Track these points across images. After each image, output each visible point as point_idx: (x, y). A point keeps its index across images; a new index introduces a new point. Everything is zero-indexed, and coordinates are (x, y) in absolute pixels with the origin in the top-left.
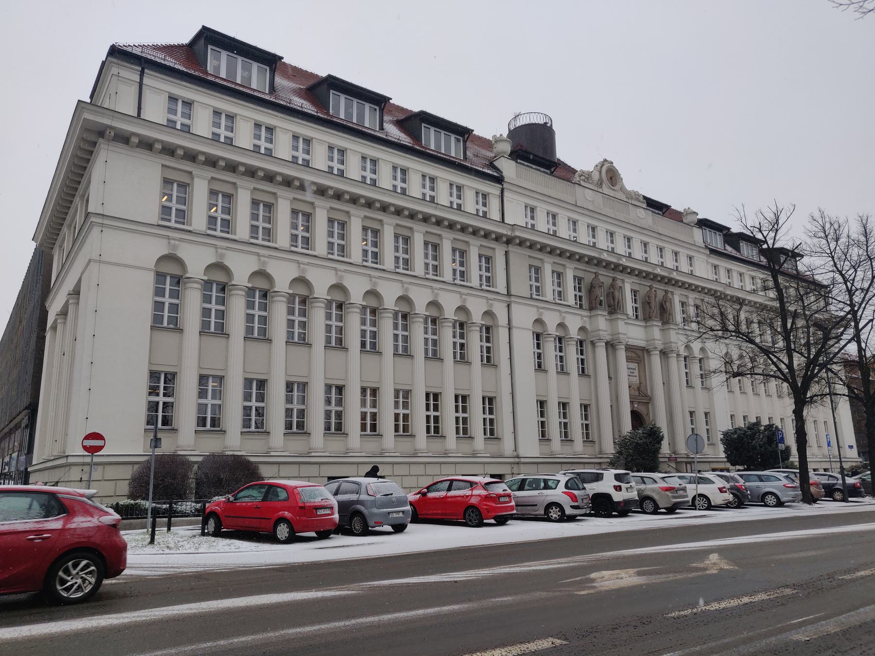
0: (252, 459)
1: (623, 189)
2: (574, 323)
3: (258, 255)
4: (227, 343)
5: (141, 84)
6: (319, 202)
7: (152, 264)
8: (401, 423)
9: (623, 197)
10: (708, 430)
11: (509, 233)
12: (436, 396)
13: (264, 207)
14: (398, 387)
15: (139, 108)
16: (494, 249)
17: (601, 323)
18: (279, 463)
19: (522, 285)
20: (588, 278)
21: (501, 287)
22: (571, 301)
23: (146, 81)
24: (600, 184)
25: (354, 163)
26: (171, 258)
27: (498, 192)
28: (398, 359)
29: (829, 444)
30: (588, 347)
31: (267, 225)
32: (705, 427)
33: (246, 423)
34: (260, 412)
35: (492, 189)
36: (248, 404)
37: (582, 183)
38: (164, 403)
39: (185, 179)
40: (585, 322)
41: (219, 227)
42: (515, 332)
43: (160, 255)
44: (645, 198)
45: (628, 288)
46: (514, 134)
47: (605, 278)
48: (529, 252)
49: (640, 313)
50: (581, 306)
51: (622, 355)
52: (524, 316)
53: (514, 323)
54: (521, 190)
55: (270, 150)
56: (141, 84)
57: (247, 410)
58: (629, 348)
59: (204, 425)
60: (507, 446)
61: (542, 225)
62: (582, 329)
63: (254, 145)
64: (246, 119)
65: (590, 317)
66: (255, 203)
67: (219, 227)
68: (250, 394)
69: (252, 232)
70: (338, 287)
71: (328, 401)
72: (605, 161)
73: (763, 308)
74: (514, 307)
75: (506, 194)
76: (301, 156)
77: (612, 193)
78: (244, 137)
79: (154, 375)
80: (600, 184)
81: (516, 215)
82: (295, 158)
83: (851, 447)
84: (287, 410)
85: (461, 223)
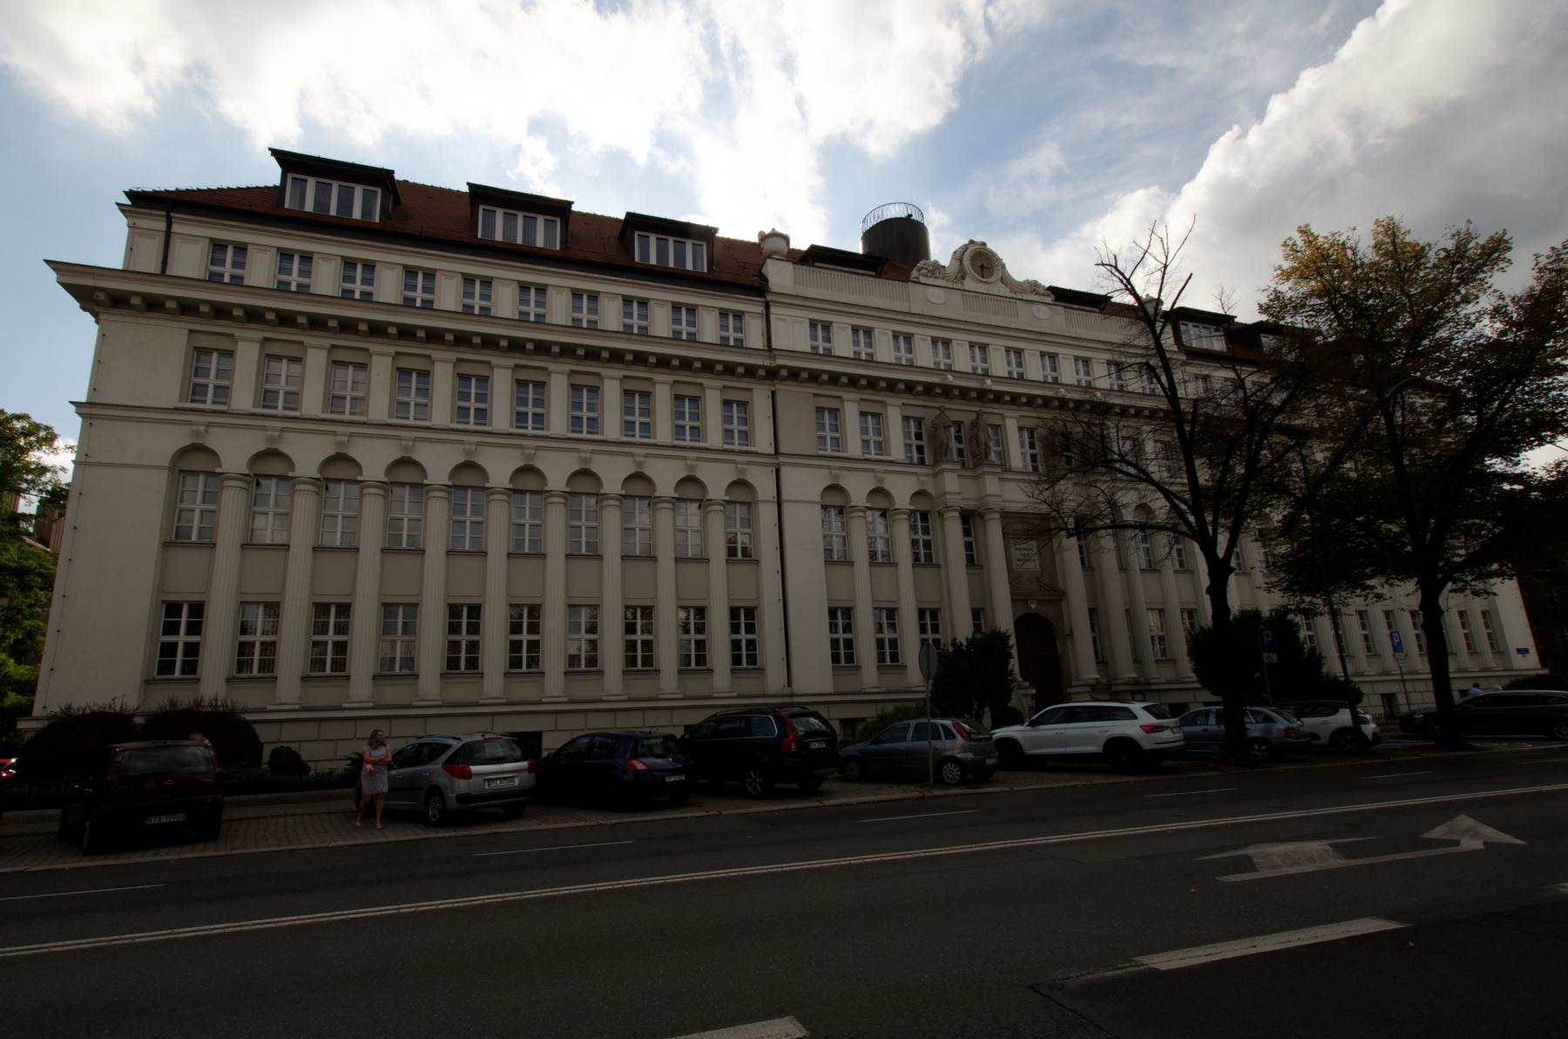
0: (249, 717)
1: (1005, 279)
2: (902, 490)
3: (829, 467)
4: (423, 561)
5: (168, 234)
6: (436, 353)
7: (818, 499)
8: (887, 650)
9: (1005, 291)
10: (1366, 637)
11: (767, 363)
12: (935, 614)
13: (687, 402)
14: (736, 604)
15: (165, 263)
16: (751, 390)
17: (953, 486)
18: (1159, 691)
19: (799, 438)
20: (929, 416)
21: (763, 442)
22: (897, 451)
23: (176, 228)
24: (962, 275)
25: (609, 306)
26: (834, 488)
27: (760, 309)
28: (876, 569)
29: (1397, 648)
30: (933, 521)
31: (743, 428)
32: (1484, 632)
33: (736, 660)
34: (849, 644)
35: (751, 307)
36: (534, 637)
37: (922, 279)
38: (263, 644)
39: (424, 366)
40: (923, 483)
41: (637, 433)
42: (786, 508)
43: (255, 451)
44: (1052, 289)
45: (1011, 427)
46: (871, 236)
47: (962, 412)
48: (811, 389)
49: (927, 455)
50: (922, 462)
51: (994, 532)
52: (804, 484)
53: (785, 496)
54: (795, 301)
55: (741, 341)
56: (168, 234)
57: (736, 645)
58: (1006, 516)
59: (740, 663)
60: (774, 679)
61: (843, 344)
62: (920, 494)
63: (521, 313)
64: (328, 257)
65: (935, 475)
66: (727, 403)
67: (637, 433)
68: (836, 625)
69: (725, 437)
70: (878, 491)
71: (923, 629)
72: (972, 242)
73: (1153, 413)
74: (784, 471)
75: (773, 309)
76: (732, 335)
77: (982, 288)
78: (709, 329)
79: (833, 613)
80: (962, 275)
81: (792, 334)
82: (815, 348)
83: (1523, 651)
84: (513, 643)
85: (924, 384)
